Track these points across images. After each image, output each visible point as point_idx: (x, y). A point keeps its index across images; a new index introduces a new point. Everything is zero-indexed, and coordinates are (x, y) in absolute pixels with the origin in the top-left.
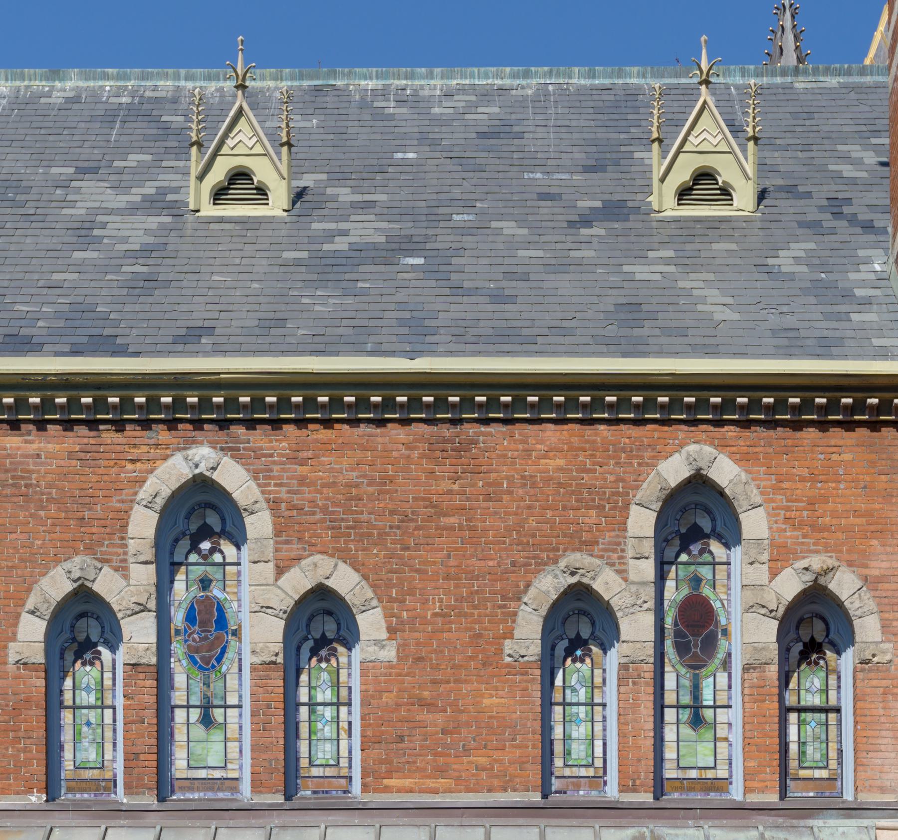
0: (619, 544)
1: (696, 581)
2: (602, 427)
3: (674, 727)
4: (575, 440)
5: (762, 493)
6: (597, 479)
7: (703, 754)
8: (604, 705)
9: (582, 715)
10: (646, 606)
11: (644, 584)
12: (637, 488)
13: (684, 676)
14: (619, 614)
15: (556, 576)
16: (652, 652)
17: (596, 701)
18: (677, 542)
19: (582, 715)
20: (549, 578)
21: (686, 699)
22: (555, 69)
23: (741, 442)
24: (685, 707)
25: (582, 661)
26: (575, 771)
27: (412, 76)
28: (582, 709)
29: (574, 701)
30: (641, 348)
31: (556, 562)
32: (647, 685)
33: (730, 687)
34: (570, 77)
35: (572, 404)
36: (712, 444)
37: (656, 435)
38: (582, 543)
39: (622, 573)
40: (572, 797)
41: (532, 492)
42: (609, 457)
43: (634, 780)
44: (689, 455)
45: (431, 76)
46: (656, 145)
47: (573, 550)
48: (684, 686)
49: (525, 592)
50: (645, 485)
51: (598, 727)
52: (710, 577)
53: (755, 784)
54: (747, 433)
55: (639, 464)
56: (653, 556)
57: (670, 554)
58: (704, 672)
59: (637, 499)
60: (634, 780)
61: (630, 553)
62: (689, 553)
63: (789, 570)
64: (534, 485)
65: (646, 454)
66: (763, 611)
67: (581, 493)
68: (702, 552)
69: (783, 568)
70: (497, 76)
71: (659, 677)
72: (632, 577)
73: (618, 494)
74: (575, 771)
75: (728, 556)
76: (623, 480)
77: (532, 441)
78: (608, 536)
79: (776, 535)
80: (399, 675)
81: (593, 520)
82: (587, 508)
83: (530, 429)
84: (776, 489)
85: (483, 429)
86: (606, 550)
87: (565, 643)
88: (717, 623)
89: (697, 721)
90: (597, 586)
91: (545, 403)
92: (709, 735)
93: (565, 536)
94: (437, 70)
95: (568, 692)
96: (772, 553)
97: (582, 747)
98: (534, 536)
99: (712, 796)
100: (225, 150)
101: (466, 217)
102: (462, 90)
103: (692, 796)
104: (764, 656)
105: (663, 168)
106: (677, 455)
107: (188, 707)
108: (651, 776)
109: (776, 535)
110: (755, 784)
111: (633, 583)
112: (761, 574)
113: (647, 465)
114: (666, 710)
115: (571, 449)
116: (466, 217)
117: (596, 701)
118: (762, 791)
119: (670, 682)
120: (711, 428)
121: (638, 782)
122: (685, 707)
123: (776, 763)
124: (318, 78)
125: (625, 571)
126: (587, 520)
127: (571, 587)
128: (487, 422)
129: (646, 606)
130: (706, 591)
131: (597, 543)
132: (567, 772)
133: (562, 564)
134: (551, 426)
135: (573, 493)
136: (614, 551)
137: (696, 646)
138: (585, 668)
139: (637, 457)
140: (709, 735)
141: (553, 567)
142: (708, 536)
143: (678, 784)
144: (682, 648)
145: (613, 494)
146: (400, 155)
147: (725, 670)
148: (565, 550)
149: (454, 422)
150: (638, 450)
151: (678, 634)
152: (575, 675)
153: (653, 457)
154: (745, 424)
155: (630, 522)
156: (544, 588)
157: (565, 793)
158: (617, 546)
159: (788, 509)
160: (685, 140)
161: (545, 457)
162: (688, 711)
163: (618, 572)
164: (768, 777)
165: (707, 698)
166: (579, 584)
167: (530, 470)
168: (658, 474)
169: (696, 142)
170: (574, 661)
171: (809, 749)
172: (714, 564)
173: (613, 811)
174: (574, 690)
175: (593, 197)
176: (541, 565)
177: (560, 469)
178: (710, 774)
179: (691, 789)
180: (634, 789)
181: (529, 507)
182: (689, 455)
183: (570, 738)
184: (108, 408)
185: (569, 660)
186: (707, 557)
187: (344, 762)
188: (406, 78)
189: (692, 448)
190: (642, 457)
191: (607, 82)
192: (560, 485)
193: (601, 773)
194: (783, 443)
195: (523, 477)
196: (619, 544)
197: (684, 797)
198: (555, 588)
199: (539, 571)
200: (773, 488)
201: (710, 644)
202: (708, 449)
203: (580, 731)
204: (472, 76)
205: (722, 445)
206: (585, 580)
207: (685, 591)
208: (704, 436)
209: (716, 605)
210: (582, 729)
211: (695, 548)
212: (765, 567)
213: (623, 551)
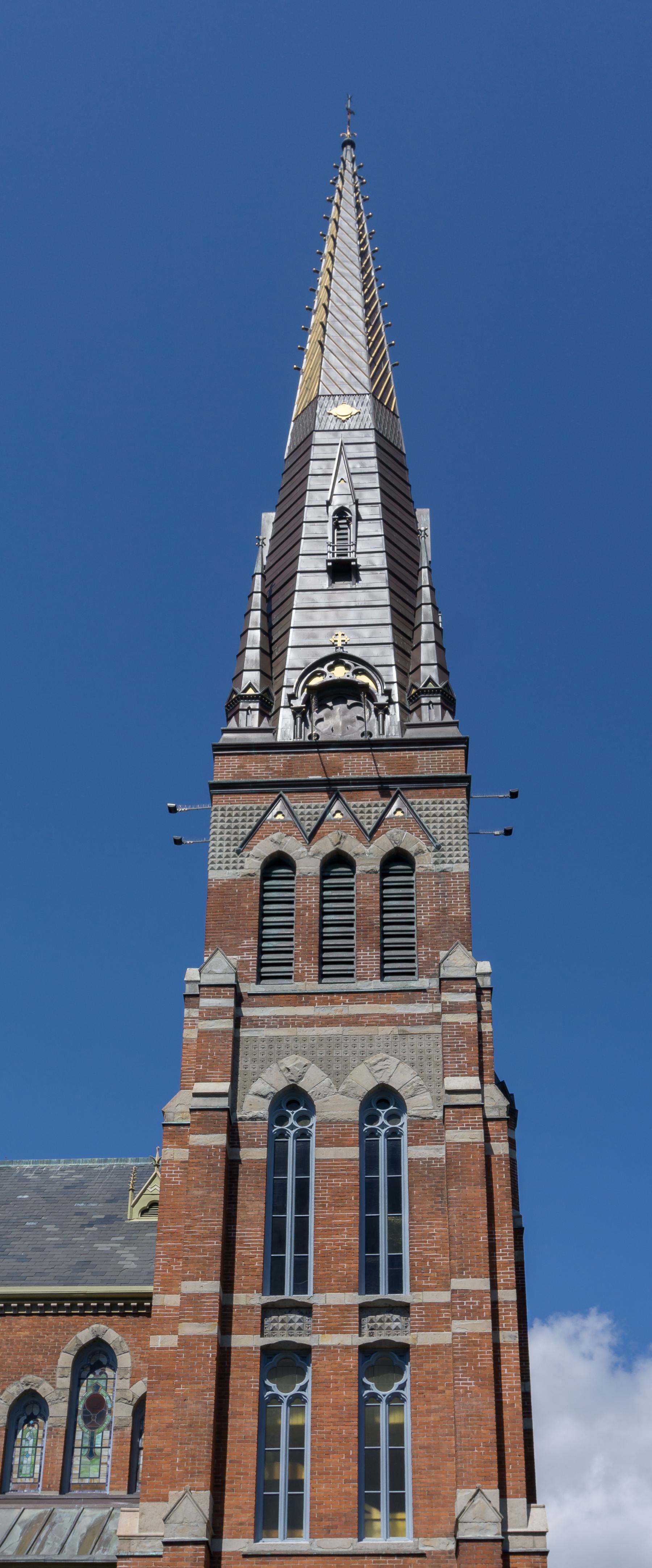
0: (53, 1370)
1: (97, 1387)
2: (50, 1317)
3: (79, 1458)
4: (36, 1323)
5: (129, 1346)
6: (45, 1341)
7: (93, 1471)
8: (42, 1447)
9: (30, 1452)
10: (64, 1400)
11: (64, 1389)
12: (65, 1344)
13: (86, 1433)
14: (49, 1404)
15: (18, 1386)
16: (65, 1421)
17: (38, 1445)
18: (89, 1369)
19: (30, 1452)
20: (15, 1387)
21: (86, 1444)
22: (119, 1159)
23: (121, 1323)
24: (85, 1448)
25: (33, 1426)
26: (23, 1480)
27: (50, 1163)
28: (30, 1449)
29: (27, 1445)
30: (77, 1281)
31: (19, 1379)
32: (61, 1437)
33: (110, 1438)
34: (127, 1162)
35: (34, 1307)
36: (105, 1324)
37: (77, 1320)
38: (33, 1370)
39: (53, 1384)
40: (20, 1493)
41: (11, 1347)
42: (53, 1331)
43: (49, 1485)
44: (93, 1329)
45: (59, 1162)
46: (131, 1192)
47: (29, 1374)
48: (86, 1438)
50: (69, 1343)
51: (38, 1458)
52: (104, 1385)
53: (115, 1486)
54: (124, 1319)
55: (67, 1334)
57: (84, 1374)
58: (97, 1430)
59: (64, 1350)
60: (49, 1485)
61: (58, 1375)
62: (94, 1374)
63: (140, 1382)
64: (12, 1344)
65: (72, 1329)
66: (125, 1401)
67: (36, 1347)
68: (101, 1374)
69: (137, 1381)
70: (91, 1162)
72: (58, 1386)
73: (55, 1347)
74: (23, 1480)
75: (115, 1375)
76: (58, 1341)
77: (13, 1324)
78: (48, 1367)
79: (135, 1365)
81: (41, 1360)
82: (39, 1354)
83: (13, 1318)
84: (137, 1344)
86: (45, 1373)
87: (25, 1418)
88: (106, 1407)
89: (91, 1454)
90: (39, 1390)
91: (20, 1307)
92: (97, 1461)
93: (25, 1367)
94: (62, 1160)
95: (24, 1441)
96: (132, 1374)
97: (28, 1468)
98: (9, 1367)
99: (96, 1492)
100: (146, 1192)
101: (32, 1223)
102: (71, 1168)
103: (85, 1492)
104: (124, 1423)
105: (134, 1201)
106: (87, 1329)
107: (82, 1448)
108: (59, 1482)
109: (135, 1365)
110: (115, 1486)
111: (58, 1389)
112: (126, 1383)
113: (71, 1334)
114: (75, 1449)
115: (33, 1327)
116: (32, 1223)
117: (38, 1445)
118: (118, 1489)
119: (79, 1435)
120: (106, 1317)
121: (51, 1486)
122: (85, 1448)
123: (127, 1475)
124: (4, 1164)
125: (55, 1383)
126: (37, 1360)
127: (26, 1391)
129: (64, 1400)
130: (102, 1392)
131: (41, 1370)
132: (19, 1480)
133: (22, 1380)
134: (24, 1317)
135: (31, 1347)
136: (50, 1374)
137: (94, 1418)
138: (34, 1429)
139: (67, 1330)
140: (97, 1461)
141: (17, 1382)
142: (105, 1366)
143: (78, 1486)
144: (86, 1419)
145: (52, 1347)
146: (20, 1197)
147: (108, 1430)
148: (24, 1374)
150: (68, 1327)
151: (85, 1412)
152: (28, 1433)
153: (74, 1330)
154: (123, 1315)
155: (60, 1360)
156: (11, 1392)
158: (52, 1372)
159: (143, 1353)
160: (145, 1189)
161: (19, 1331)
162: (87, 1450)
163: (51, 1384)
164: (122, 1482)
165: (98, 1443)
166: (30, 1390)
167: (11, 1337)
168: (77, 1338)
169: (151, 1190)
170: (29, 1426)
171: (24, 1468)
172: (107, 1379)
173: (36, 1501)
174: (27, 1440)
175: (100, 1213)
176: (11, 1381)
178: (96, 1481)
179: (85, 1488)
180: (49, 1489)
181: (8, 1354)
182: (93, 1329)
183: (22, 1463)
184: (118, 1308)
185: (26, 1426)
186: (103, 1376)
187: (36, 1476)
188: (47, 1163)
189: (95, 1326)
190: (69, 1331)
191: (143, 1163)
192: (25, 1343)
193: (37, 1481)
194: (142, 1323)
195: (7, 1340)
196: (53, 1370)
197: (81, 1492)
198: (18, 1392)
199: (10, 1384)
200: (135, 1343)
201: (101, 1417)
202: (103, 1326)
203: (27, 1460)
204: (79, 1162)
205: (111, 1325)
206: (33, 1388)
207: (91, 1392)
208: (102, 1320)
209: (107, 1398)
210: (29, 1459)
211: (97, 1372)
212: (128, 1381)
213: (54, 1374)
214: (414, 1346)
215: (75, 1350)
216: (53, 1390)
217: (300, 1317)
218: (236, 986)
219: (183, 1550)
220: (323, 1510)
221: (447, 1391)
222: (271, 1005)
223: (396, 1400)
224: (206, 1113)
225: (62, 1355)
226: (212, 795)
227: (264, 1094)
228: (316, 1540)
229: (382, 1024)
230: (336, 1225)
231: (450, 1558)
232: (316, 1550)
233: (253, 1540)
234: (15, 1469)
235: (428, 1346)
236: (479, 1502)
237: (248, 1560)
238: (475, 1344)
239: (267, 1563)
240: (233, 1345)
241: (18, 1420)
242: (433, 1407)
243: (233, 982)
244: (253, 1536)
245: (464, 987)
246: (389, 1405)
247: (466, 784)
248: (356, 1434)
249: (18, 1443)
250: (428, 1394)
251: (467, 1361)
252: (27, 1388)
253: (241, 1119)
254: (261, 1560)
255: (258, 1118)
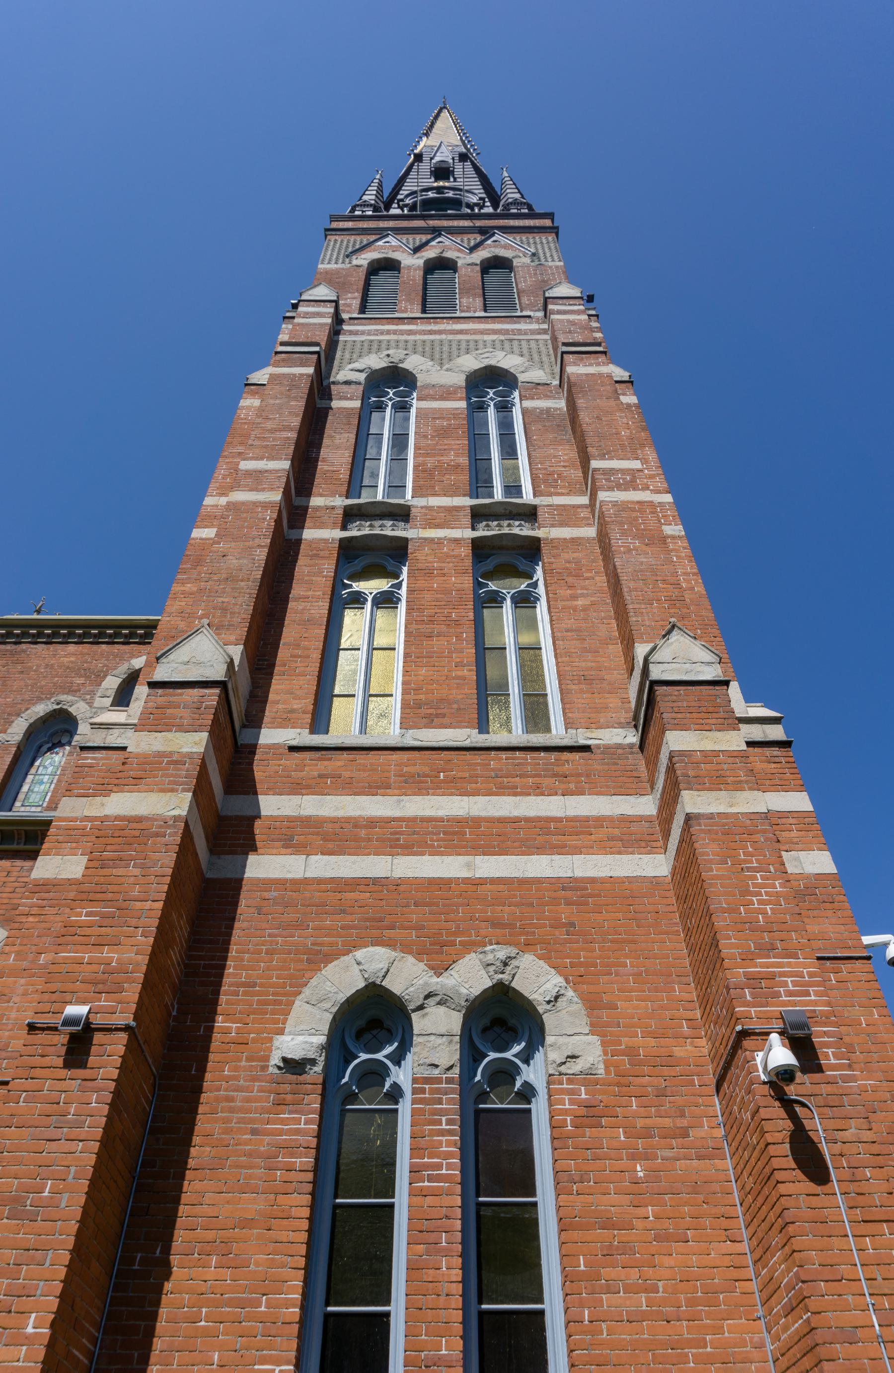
14: (79, 722)
31: (50, 699)
49: (24, 712)
56: (112, 697)
71: (649, 717)
76: (107, 666)
80: (546, 764)
85: (32, 646)
95: (41, 768)
111: (95, 708)
127: (55, 710)
128: (36, 643)
133: (52, 700)
149: (15, 643)
155: (104, 683)
157: (218, 1217)
171: (33, 796)
176: (40, 699)
177: (72, 662)
199: (37, 703)
206: (65, 707)
210: (42, 787)
214: (547, 539)
215: (125, 674)
216: (89, 708)
217: (391, 522)
218: (336, 302)
219: (181, 695)
220: (422, 697)
221: (597, 578)
222: (373, 324)
223: (525, 600)
224: (291, 355)
225: (109, 678)
226: (326, 236)
227: (361, 368)
228: (411, 731)
229: (489, 334)
230: (440, 450)
231: (632, 753)
232: (409, 742)
233: (308, 730)
234: (21, 796)
235: (565, 539)
236: (677, 640)
237: (296, 754)
238: (633, 510)
239: (330, 759)
240: (304, 537)
241: (40, 747)
242: (579, 592)
243: (335, 298)
244: (308, 726)
245: (571, 303)
246: (516, 607)
247: (556, 230)
248: (472, 618)
249: (33, 771)
250: (570, 580)
251: (625, 524)
252: (59, 707)
253: (334, 383)
254: (318, 754)
255: (353, 382)
